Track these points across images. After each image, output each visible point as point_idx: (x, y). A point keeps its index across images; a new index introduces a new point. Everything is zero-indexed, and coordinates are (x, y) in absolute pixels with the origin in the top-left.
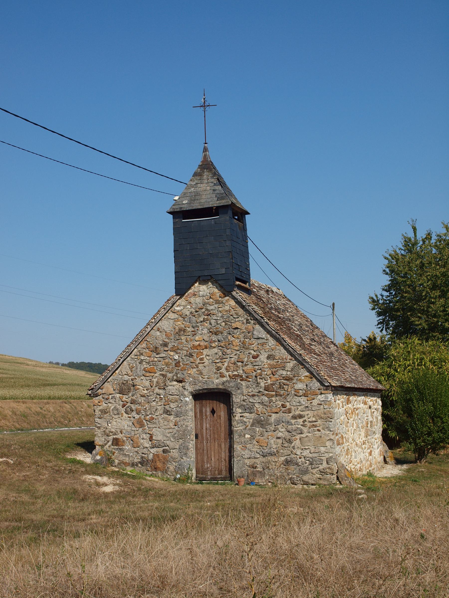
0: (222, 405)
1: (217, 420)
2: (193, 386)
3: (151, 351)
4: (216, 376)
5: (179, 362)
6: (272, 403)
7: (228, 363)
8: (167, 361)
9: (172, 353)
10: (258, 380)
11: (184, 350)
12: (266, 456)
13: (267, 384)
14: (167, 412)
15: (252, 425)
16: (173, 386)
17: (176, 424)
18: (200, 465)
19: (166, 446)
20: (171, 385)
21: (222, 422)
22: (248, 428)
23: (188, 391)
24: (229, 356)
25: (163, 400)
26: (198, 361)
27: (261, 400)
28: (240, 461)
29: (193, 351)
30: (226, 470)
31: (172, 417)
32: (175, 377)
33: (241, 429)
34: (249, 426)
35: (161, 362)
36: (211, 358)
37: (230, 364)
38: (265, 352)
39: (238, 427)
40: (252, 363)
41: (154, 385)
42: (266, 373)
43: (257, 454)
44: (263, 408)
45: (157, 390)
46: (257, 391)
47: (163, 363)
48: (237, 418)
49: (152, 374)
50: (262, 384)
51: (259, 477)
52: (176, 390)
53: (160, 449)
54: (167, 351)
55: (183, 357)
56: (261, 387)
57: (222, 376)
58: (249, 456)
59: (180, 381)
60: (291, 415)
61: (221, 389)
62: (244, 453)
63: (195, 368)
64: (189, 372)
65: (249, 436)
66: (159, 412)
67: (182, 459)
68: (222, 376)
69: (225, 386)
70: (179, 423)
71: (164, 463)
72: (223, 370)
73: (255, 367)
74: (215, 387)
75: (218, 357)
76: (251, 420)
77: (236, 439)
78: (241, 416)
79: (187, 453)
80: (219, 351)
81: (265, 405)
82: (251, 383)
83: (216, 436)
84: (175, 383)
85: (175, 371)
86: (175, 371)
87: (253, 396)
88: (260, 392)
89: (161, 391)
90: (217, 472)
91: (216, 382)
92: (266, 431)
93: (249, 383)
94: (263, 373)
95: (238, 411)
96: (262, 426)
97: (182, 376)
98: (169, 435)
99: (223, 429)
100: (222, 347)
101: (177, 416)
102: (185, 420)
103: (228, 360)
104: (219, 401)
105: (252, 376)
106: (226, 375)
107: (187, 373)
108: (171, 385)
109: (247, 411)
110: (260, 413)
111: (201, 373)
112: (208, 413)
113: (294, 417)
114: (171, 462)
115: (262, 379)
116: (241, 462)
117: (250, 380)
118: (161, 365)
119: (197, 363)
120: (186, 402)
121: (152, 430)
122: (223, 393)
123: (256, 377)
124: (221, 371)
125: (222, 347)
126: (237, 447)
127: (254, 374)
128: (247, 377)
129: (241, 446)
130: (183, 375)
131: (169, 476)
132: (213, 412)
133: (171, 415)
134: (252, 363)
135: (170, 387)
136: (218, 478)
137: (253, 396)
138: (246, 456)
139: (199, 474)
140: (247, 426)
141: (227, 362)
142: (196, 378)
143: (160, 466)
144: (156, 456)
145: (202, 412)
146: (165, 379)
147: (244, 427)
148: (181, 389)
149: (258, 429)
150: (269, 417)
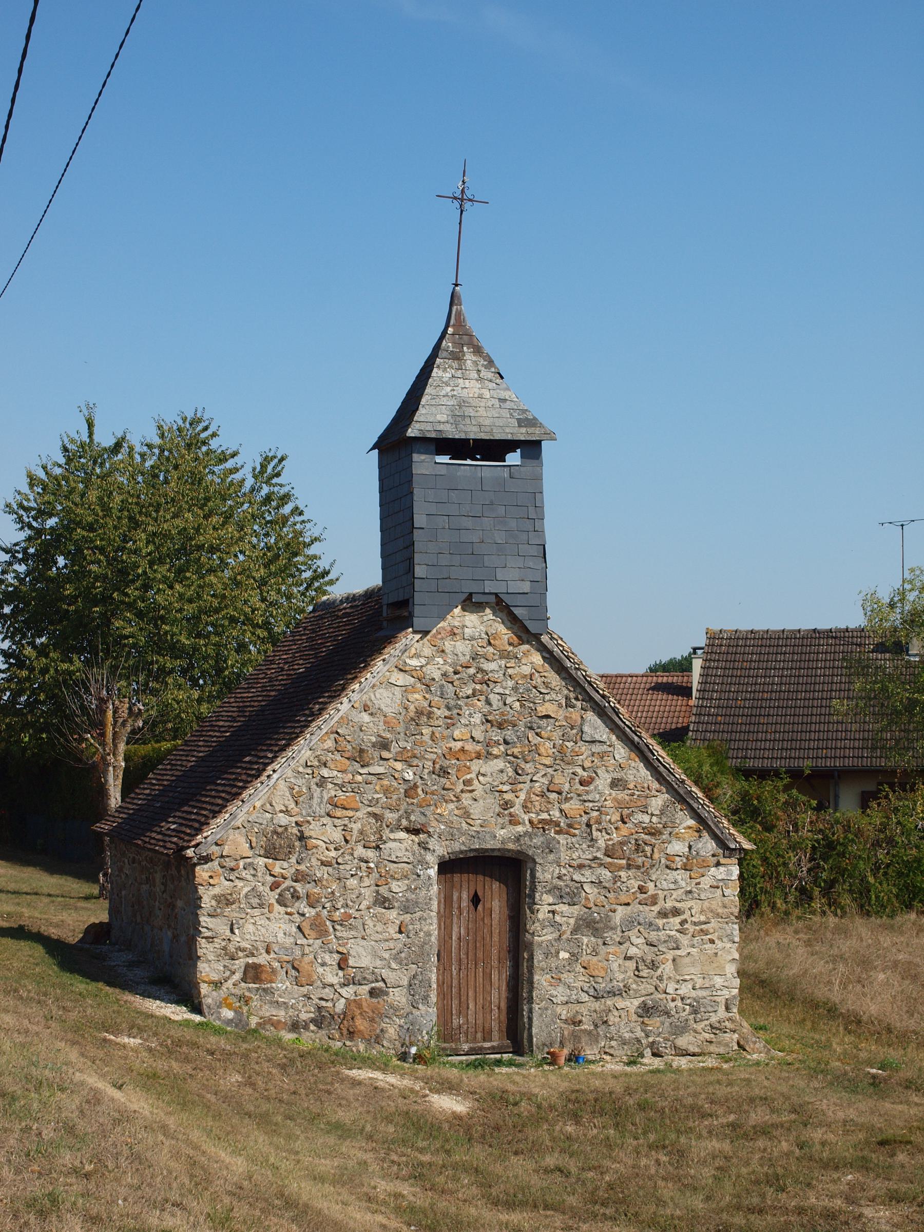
0: (496, 885)
2: (447, 842)
4: (500, 820)
5: (415, 786)
6: (619, 884)
9: (399, 766)
10: (594, 833)
12: (603, 997)
13: (610, 843)
14: (383, 902)
15: (575, 931)
16: (400, 841)
19: (377, 981)
20: (395, 840)
21: (495, 922)
22: (564, 937)
23: (436, 854)
28: (546, 1009)
29: (448, 762)
30: (500, 1030)
31: (393, 914)
32: (404, 823)
33: (550, 940)
34: (569, 933)
35: (371, 786)
37: (532, 796)
39: (542, 936)
40: (579, 795)
41: (354, 838)
43: (583, 995)
44: (599, 893)
45: (360, 851)
46: (590, 857)
47: (377, 788)
48: (540, 916)
50: (601, 843)
51: (586, 1044)
52: (407, 850)
55: (426, 777)
56: (599, 849)
57: (514, 821)
58: (565, 999)
59: (416, 832)
60: (656, 908)
61: (509, 851)
62: (555, 993)
64: (439, 811)
65: (567, 955)
67: (414, 1011)
68: (514, 821)
69: (521, 845)
70: (411, 927)
71: (372, 1020)
72: (517, 809)
73: (587, 804)
74: (499, 846)
75: (506, 779)
76: (572, 921)
77: (539, 962)
78: (549, 912)
80: (508, 765)
81: (605, 887)
82: (578, 838)
84: (402, 835)
85: (404, 807)
86: (404, 807)
87: (581, 866)
88: (596, 858)
89: (370, 854)
90: (479, 1035)
91: (501, 836)
92: (604, 944)
93: (574, 840)
94: (603, 817)
95: (545, 902)
97: (422, 820)
98: (386, 955)
99: (496, 938)
100: (516, 757)
101: (406, 910)
102: (425, 920)
104: (491, 877)
108: (395, 840)
109: (564, 901)
110: (592, 905)
111: (467, 815)
113: (663, 914)
114: (390, 1018)
115: (600, 831)
116: (549, 1012)
117: (577, 832)
118: (374, 792)
119: (459, 790)
121: (347, 943)
123: (589, 825)
124: (512, 810)
125: (516, 757)
126: (541, 980)
127: (585, 819)
128: (570, 826)
129: (548, 976)
130: (423, 818)
132: (476, 900)
134: (579, 795)
135: (390, 845)
137: (581, 866)
138: (560, 999)
140: (564, 932)
141: (525, 791)
143: (362, 1028)
144: (353, 1004)
146: (381, 826)
148: (416, 847)
149: (585, 940)
150: (610, 913)
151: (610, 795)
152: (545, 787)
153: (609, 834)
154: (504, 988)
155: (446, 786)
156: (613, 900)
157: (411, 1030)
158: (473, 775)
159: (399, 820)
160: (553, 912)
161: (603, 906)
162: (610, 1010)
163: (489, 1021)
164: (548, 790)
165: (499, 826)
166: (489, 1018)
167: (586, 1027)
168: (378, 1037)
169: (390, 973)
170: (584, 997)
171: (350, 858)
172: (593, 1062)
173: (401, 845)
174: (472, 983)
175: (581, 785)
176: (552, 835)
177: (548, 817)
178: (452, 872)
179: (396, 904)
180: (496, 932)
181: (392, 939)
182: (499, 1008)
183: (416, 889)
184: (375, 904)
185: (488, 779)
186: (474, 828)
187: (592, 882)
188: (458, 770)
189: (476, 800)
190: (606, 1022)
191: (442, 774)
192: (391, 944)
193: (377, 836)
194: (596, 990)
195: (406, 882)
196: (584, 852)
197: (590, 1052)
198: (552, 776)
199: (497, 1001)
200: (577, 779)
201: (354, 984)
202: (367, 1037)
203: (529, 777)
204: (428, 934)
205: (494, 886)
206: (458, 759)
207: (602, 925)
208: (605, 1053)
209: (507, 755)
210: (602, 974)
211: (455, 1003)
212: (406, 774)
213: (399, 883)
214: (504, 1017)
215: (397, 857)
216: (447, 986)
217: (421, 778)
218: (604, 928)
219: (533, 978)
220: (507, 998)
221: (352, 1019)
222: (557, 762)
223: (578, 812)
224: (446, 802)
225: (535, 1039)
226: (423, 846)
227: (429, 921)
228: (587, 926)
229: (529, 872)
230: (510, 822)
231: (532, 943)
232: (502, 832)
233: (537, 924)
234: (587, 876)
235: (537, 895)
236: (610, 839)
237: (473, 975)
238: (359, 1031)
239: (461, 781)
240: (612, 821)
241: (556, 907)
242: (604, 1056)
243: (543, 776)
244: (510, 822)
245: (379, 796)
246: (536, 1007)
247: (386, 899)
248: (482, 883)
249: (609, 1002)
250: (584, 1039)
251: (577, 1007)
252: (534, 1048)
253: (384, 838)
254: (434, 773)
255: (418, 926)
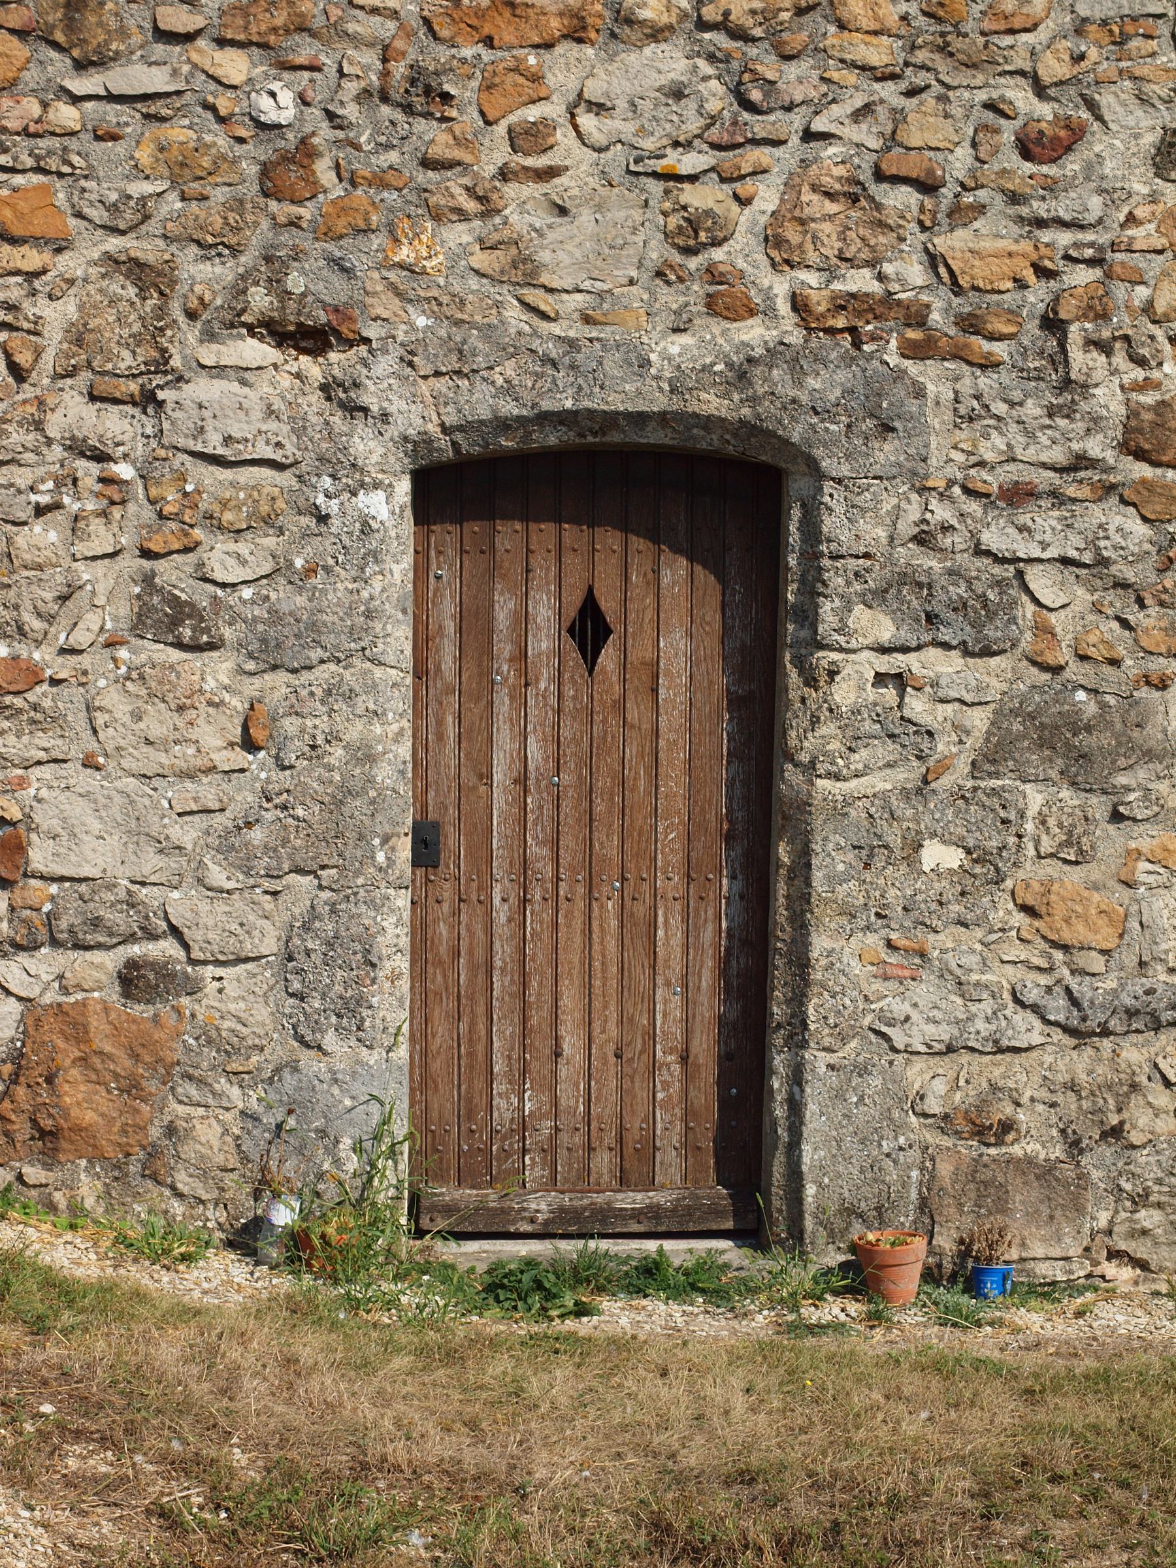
0: (675, 572)
1: (620, 706)
2: (442, 384)
3: (21, 34)
4: (669, 297)
5: (306, 151)
7: (790, 185)
8: (178, 133)
9: (234, 65)
10: (1078, 358)
11: (355, 40)
12: (1106, 1032)
13: (1149, 398)
14: (172, 620)
15: (989, 760)
16: (242, 374)
17: (257, 733)
18: (445, 1100)
19: (153, 937)
20: (218, 371)
21: (672, 719)
22: (945, 782)
23: (392, 431)
24: (797, 120)
25: (139, 511)
26: (496, 152)
27: (1092, 543)
28: (863, 1070)
29: (443, 53)
30: (689, 1147)
31: (217, 671)
32: (260, 300)
33: (883, 796)
34: (962, 766)
35: (120, 148)
36: (628, 129)
37: (807, 196)
38: (1143, 99)
39: (845, 773)
40: (1015, 198)
41: (48, 361)
42: (1142, 293)
43: (1022, 1019)
44: (1097, 608)
45: (73, 412)
46: (1057, 455)
47: (144, 155)
48: (844, 694)
49: (31, 258)
50: (1108, 399)
51: (1032, 1216)
52: (271, 412)
53: (96, 956)
54: (188, 38)
55: (351, 111)
56: (1095, 423)
57: (727, 301)
58: (944, 1033)
59: (309, 339)
61: (708, 423)
62: (900, 1008)
63: (462, 215)
64: (404, 253)
65: (953, 858)
66: (92, 620)
67: (306, 1057)
68: (727, 301)
69: (754, 400)
70: (290, 725)
71: (132, 1088)
72: (741, 252)
73: (1046, 236)
74: (659, 402)
75: (694, 125)
76: (979, 720)
77: (834, 880)
78: (880, 679)
79: (360, 1000)
80: (706, 68)
82: (1005, 376)
83: (608, 846)
84: (255, 351)
85: (258, 236)
86: (258, 236)
87: (1017, 495)
88: (1080, 462)
89: (116, 425)
90: (603, 1162)
91: (667, 361)
92: (1116, 817)
93: (986, 382)
94: (1120, 291)
95: (859, 636)
96: (1080, 767)
97: (336, 289)
98: (186, 834)
99: (674, 782)
100: (740, 35)
101: (268, 655)
102: (350, 696)
103: (787, 157)
104: (655, 538)
105: (1013, 314)
106: (769, 297)
107: (385, 265)
108: (218, 371)
109: (945, 635)
110: (1064, 655)
111: (523, 271)
112: (543, 641)
114: (201, 1082)
115: (1105, 348)
116: (876, 1081)
117: (1000, 349)
118: (125, 170)
119: (490, 170)
120: (366, 529)
121: (22, 783)
122: (658, 455)
123: (1053, 324)
124: (718, 254)
125: (740, 35)
126: (843, 955)
127: (1038, 295)
128: (970, 324)
129: (872, 939)
130: (338, 281)
131: (177, 1208)
132: (589, 629)
133: (211, 647)
134: (1015, 198)
135: (202, 389)
136: (623, 1215)
137: (1017, 495)
138: (919, 1034)
139: (440, 1176)
140: (944, 766)
141: (776, 179)
142: (473, 312)
143: (90, 1117)
144: (49, 1023)
145: (490, 630)
146: (161, 311)
147: (908, 774)
148: (313, 402)
149: (1035, 798)
150: (1144, 693)
151: (1153, 198)
152: (866, 163)
153: (1141, 362)
154: (707, 978)
155: (436, 152)
156: (1155, 639)
157: (285, 1129)
158: (554, 110)
159: (239, 291)
160: (900, 680)
161: (1114, 662)
162: (1134, 1087)
163: (642, 1110)
164: (879, 176)
165: (664, 321)
166: (643, 1095)
167: (1031, 1147)
168: (153, 1153)
169: (204, 907)
170: (1025, 1029)
171: (31, 438)
172: (1047, 1291)
173: (244, 391)
174: (572, 956)
175: (1026, 155)
176: (893, 359)
177: (875, 287)
178: (490, 513)
179: (228, 633)
180: (674, 759)
181: (213, 769)
182: (684, 1059)
183: (310, 571)
184: (138, 626)
185: (619, 125)
186: (556, 329)
187: (1065, 561)
188: (488, 87)
189: (562, 211)
190: (1116, 1132)
191: (418, 102)
192: (208, 791)
193: (146, 353)
194: (1074, 1002)
195: (270, 542)
196: (1030, 435)
197: (1039, 1246)
198: (899, 117)
199: (677, 1031)
200: (1008, 132)
201: (55, 943)
202: (110, 1151)
203: (797, 120)
204: (365, 755)
205: (666, 576)
206: (489, 42)
207: (1105, 740)
208: (1114, 1255)
209: (703, 25)
210: (1105, 937)
211: (504, 1034)
212: (265, 102)
213: (243, 548)
214: (706, 1095)
215: (228, 440)
216: (473, 969)
217: (330, 116)
218: (1113, 754)
219: (807, 945)
220: (722, 1020)
221: (49, 1080)
222: (921, 56)
223: (1007, 266)
224: (437, 217)
225: (810, 1190)
226: (342, 396)
227: (365, 702)
228: (1042, 744)
229: (796, 513)
230: (712, 305)
231: (804, 806)
232: (676, 345)
233: (828, 729)
234: (1047, 532)
235: (827, 610)
236: (1147, 385)
237: (578, 923)
238: (78, 1129)
239: (501, 129)
240: (1160, 307)
241: (911, 662)
242: (1109, 1269)
243: (859, 115)
244: (712, 305)
245: (148, 188)
246: (818, 1060)
247: (181, 611)
248: (614, 560)
249: (1134, 1054)
250: (1022, 1197)
251: (996, 1069)
252: (809, 1223)
253: (176, 362)
254: (385, 98)
255: (323, 724)
